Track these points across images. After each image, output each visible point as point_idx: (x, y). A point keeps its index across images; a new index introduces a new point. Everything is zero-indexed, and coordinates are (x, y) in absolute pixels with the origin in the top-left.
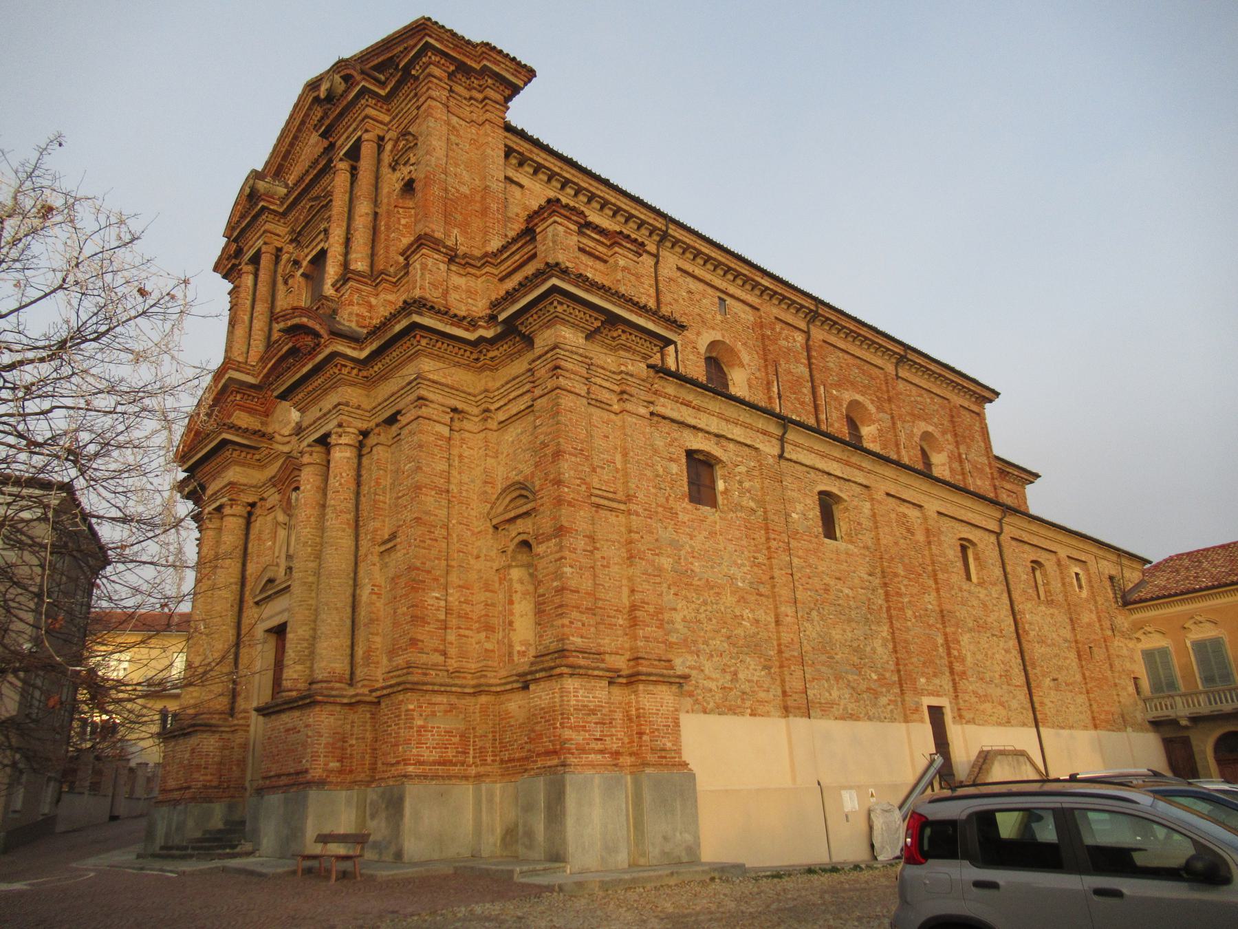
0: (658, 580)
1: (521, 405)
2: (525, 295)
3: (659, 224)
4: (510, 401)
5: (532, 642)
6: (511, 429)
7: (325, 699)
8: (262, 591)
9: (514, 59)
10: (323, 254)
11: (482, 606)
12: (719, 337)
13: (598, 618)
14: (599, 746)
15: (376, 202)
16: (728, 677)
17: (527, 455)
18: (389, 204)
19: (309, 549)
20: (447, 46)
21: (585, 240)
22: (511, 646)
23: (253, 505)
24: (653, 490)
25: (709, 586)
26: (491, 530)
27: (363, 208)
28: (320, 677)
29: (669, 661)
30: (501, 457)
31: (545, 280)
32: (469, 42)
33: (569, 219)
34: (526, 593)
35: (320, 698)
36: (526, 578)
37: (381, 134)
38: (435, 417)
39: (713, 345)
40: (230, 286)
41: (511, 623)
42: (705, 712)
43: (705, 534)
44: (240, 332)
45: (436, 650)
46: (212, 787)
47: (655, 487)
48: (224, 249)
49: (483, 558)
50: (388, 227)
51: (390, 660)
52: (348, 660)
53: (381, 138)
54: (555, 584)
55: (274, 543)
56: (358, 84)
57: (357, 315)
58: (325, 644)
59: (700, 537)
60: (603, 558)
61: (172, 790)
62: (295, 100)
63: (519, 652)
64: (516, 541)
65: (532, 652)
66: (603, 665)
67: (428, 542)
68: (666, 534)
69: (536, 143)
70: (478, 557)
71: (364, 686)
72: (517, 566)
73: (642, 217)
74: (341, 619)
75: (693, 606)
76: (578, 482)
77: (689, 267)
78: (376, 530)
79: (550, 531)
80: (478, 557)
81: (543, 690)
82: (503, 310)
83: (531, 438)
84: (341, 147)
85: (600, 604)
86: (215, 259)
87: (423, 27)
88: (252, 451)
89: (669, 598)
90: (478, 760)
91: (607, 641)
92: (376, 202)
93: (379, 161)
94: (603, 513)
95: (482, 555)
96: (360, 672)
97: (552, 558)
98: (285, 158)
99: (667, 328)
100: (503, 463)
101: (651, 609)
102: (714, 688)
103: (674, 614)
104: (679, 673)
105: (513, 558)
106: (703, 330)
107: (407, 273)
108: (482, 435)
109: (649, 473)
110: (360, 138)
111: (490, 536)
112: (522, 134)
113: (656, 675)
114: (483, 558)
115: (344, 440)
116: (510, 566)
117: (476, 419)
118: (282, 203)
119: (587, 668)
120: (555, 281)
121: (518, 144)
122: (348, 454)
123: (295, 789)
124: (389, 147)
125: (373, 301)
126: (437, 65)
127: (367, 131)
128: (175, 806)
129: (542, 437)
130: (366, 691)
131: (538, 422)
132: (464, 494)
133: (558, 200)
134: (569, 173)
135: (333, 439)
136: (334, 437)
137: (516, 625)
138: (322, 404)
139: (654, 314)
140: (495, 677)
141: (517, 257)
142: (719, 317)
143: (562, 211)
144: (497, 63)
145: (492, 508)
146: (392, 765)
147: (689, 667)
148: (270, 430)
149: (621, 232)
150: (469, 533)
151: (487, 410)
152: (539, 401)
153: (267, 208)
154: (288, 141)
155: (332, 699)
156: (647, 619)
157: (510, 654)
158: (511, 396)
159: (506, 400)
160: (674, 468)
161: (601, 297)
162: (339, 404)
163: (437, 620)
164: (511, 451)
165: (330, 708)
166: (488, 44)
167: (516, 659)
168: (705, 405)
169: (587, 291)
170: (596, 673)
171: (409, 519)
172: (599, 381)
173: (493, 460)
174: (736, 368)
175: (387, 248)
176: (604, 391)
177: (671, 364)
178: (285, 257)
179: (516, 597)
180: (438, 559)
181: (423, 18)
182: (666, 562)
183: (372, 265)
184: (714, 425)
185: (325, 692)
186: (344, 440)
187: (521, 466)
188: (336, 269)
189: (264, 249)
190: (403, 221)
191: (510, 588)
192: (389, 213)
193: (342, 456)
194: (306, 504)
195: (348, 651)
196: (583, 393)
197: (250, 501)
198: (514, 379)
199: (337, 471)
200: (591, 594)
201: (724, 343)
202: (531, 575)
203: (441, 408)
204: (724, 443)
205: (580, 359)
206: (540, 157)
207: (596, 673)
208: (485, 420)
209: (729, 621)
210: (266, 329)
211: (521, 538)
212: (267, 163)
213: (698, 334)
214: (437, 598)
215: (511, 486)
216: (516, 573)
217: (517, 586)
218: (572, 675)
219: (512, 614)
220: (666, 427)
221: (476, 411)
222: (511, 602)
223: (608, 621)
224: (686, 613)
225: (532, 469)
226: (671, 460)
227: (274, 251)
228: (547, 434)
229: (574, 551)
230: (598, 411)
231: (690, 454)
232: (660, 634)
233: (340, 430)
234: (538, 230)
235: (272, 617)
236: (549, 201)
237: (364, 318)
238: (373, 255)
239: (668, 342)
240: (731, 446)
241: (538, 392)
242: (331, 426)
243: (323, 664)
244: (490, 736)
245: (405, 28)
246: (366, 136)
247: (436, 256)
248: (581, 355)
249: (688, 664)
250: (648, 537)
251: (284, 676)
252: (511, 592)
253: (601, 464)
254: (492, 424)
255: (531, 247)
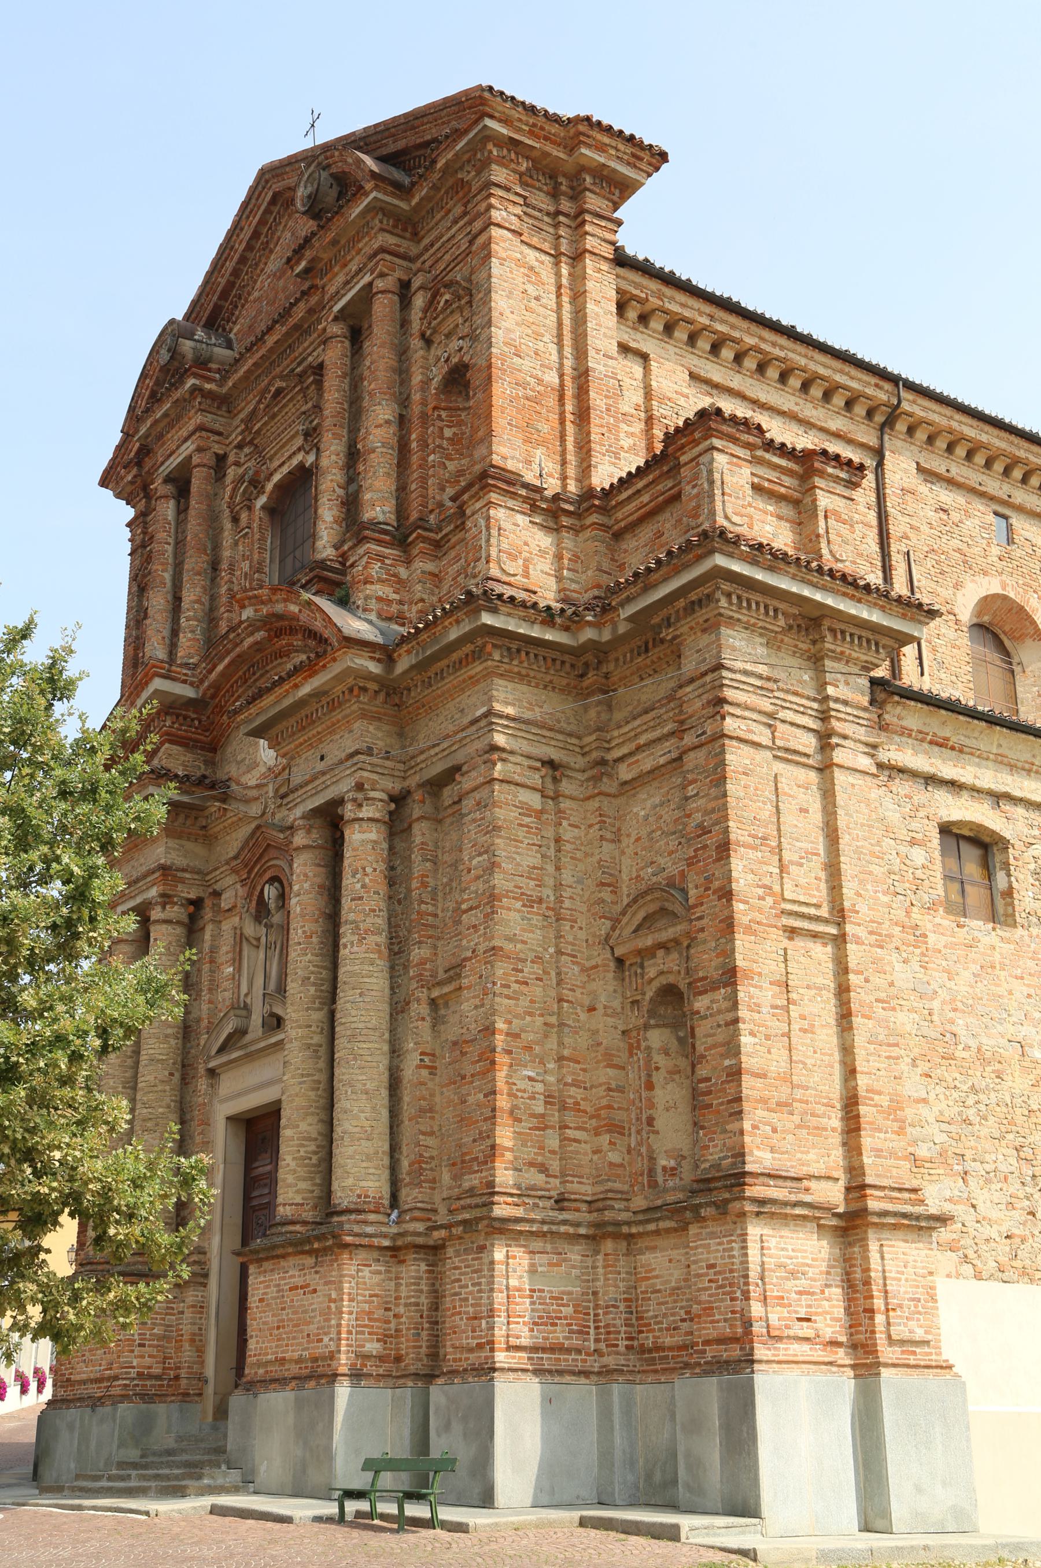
0: (895, 1052)
1: (658, 756)
2: (666, 579)
3: (882, 394)
4: (639, 748)
5: (685, 1153)
6: (643, 796)
7: (357, 1241)
8: (221, 1050)
9: (632, 137)
10: (303, 478)
11: (601, 1091)
12: (995, 588)
13: (796, 1119)
14: (805, 1330)
15: (404, 402)
16: (1019, 1215)
17: (673, 844)
18: (424, 403)
19: (312, 989)
20: (519, 130)
21: (761, 471)
22: (652, 1159)
23: (197, 904)
24: (885, 899)
25: (982, 1058)
26: (612, 965)
27: (381, 413)
28: (345, 1204)
29: (915, 1191)
30: (625, 841)
31: (699, 558)
32: (556, 119)
33: (735, 440)
34: (674, 1072)
35: (349, 1239)
36: (674, 1044)
37: (405, 278)
38: (517, 778)
39: (987, 602)
40: (129, 513)
41: (650, 1121)
42: (978, 1276)
43: (975, 968)
44: (158, 601)
45: (531, 1164)
46: (150, 1377)
47: (886, 893)
48: (118, 448)
49: (601, 1010)
50: (424, 444)
51: (455, 1178)
52: (386, 1174)
53: (405, 286)
54: (727, 1062)
55: (239, 970)
56: (367, 194)
57: (379, 599)
58: (350, 1151)
59: (966, 975)
60: (803, 1017)
61: (84, 1382)
62: (242, 196)
63: (664, 1168)
64: (656, 984)
65: (687, 1175)
66: (808, 1198)
67: (515, 986)
68: (903, 975)
69: (669, 280)
70: (592, 1009)
71: (414, 1219)
72: (657, 1026)
73: (854, 385)
74: (374, 1108)
75: (955, 1095)
76: (760, 891)
77: (938, 464)
78: (422, 962)
79: (715, 975)
80: (592, 1009)
81: (712, 1235)
82: (629, 600)
83: (678, 814)
84: (337, 296)
85: (798, 1094)
86: (104, 464)
87: (475, 103)
88: (194, 813)
89: (913, 1086)
90: (602, 1346)
91: (811, 1156)
92: (404, 402)
93: (404, 323)
94: (800, 943)
95: (600, 1007)
96: (409, 1196)
97: (721, 1019)
98: (224, 295)
99: (904, 616)
100: (629, 851)
101: (884, 1101)
102: (995, 1235)
103: (924, 1111)
104: (933, 1211)
105: (652, 1013)
106: (967, 578)
107: (461, 527)
108: (594, 804)
109: (878, 870)
110: (370, 284)
111: (611, 975)
112: (645, 268)
113: (895, 1214)
114: (601, 1010)
115: (367, 812)
116: (646, 1027)
117: (580, 776)
118: (224, 379)
119: (786, 1204)
120: (720, 560)
121: (637, 285)
122: (373, 836)
123: (313, 1383)
124: (419, 301)
125: (403, 572)
126: (502, 162)
127: (382, 275)
128: (93, 1407)
129: (698, 817)
130: (420, 1227)
131: (691, 791)
132: (567, 904)
133: (719, 412)
134: (725, 325)
135: (348, 811)
136: (349, 806)
137: (659, 1124)
138: (325, 748)
139: (883, 597)
140: (627, 1209)
141: (645, 498)
142: (995, 551)
143: (724, 428)
144: (601, 148)
145: (613, 928)
146: (471, 1350)
147: (950, 1200)
148: (221, 775)
149: (824, 452)
150: (576, 968)
151: (603, 762)
152: (692, 755)
153: (201, 390)
154: (230, 265)
155: (366, 1241)
156: (880, 1121)
157: (651, 1172)
158: (642, 740)
159: (632, 746)
160: (918, 856)
161: (794, 577)
162: (357, 752)
163: (533, 1115)
164: (644, 833)
165: (362, 1254)
166: (588, 119)
167: (660, 1179)
168: (972, 743)
169: (771, 569)
170: (798, 1211)
171: (481, 948)
172: (789, 715)
173: (612, 846)
174: (1029, 642)
175: (424, 479)
176: (799, 732)
177: (910, 677)
178: (232, 473)
179: (658, 1078)
180: (531, 1014)
181: (480, 87)
182: (904, 1020)
183: (401, 511)
184: (989, 778)
185: (356, 1229)
186: (367, 812)
187: (662, 861)
188: (335, 512)
189: (195, 460)
190: (448, 433)
191: (649, 1059)
192: (424, 417)
193: (363, 841)
194: (303, 916)
195: (386, 1161)
196: (766, 741)
197: (192, 896)
198: (646, 712)
199: (359, 864)
200: (787, 1078)
201: (1005, 598)
202: (681, 1041)
203: (526, 762)
204: (1007, 807)
205: (759, 683)
206: (677, 304)
207: (798, 1211)
208: (596, 779)
209: (1020, 1120)
210: (205, 599)
211: (663, 980)
212: (195, 304)
213: (957, 586)
214: (530, 1079)
215: (646, 893)
216: (656, 1038)
217: (659, 1059)
218: (758, 1214)
219: (651, 1105)
220: (902, 787)
221: (580, 762)
222: (650, 1086)
223: (814, 1121)
224: (943, 1106)
225: (682, 866)
226: (913, 842)
227: (213, 462)
228: (706, 813)
229: (756, 1008)
230: (791, 768)
231: (946, 830)
232: (898, 1144)
233: (360, 796)
234: (683, 459)
235: (239, 1095)
236: (702, 414)
237: (389, 602)
238: (402, 490)
239: (906, 639)
240: (1020, 811)
241: (689, 739)
242: (344, 787)
243: (350, 1181)
244: (622, 1307)
245: (446, 100)
246: (380, 284)
247: (511, 503)
248: (760, 677)
249: (948, 1194)
250: (877, 980)
251: (280, 1200)
252: (650, 1069)
253: (795, 858)
254: (608, 786)
255: (670, 483)
